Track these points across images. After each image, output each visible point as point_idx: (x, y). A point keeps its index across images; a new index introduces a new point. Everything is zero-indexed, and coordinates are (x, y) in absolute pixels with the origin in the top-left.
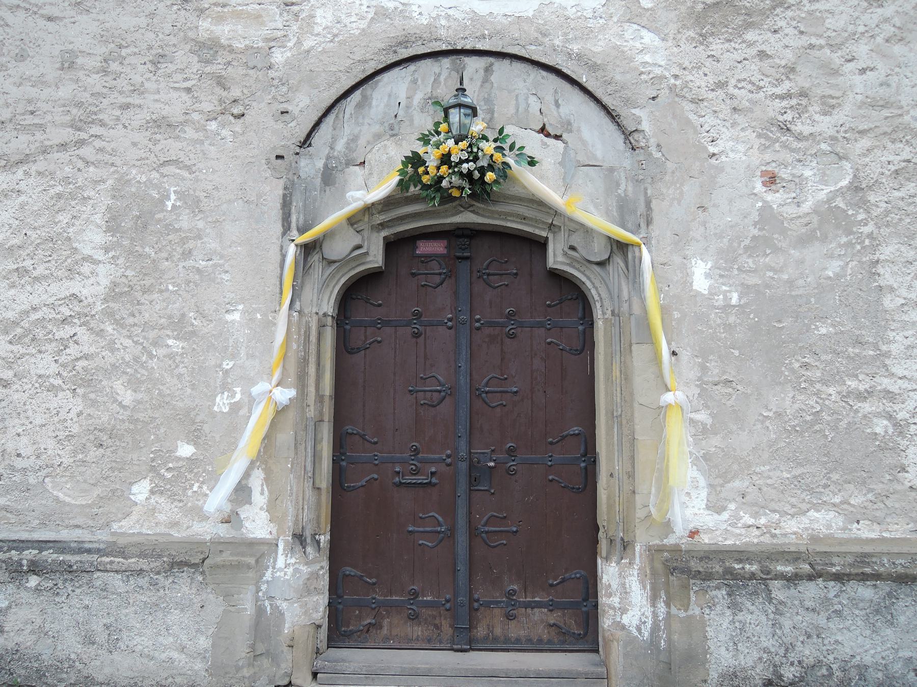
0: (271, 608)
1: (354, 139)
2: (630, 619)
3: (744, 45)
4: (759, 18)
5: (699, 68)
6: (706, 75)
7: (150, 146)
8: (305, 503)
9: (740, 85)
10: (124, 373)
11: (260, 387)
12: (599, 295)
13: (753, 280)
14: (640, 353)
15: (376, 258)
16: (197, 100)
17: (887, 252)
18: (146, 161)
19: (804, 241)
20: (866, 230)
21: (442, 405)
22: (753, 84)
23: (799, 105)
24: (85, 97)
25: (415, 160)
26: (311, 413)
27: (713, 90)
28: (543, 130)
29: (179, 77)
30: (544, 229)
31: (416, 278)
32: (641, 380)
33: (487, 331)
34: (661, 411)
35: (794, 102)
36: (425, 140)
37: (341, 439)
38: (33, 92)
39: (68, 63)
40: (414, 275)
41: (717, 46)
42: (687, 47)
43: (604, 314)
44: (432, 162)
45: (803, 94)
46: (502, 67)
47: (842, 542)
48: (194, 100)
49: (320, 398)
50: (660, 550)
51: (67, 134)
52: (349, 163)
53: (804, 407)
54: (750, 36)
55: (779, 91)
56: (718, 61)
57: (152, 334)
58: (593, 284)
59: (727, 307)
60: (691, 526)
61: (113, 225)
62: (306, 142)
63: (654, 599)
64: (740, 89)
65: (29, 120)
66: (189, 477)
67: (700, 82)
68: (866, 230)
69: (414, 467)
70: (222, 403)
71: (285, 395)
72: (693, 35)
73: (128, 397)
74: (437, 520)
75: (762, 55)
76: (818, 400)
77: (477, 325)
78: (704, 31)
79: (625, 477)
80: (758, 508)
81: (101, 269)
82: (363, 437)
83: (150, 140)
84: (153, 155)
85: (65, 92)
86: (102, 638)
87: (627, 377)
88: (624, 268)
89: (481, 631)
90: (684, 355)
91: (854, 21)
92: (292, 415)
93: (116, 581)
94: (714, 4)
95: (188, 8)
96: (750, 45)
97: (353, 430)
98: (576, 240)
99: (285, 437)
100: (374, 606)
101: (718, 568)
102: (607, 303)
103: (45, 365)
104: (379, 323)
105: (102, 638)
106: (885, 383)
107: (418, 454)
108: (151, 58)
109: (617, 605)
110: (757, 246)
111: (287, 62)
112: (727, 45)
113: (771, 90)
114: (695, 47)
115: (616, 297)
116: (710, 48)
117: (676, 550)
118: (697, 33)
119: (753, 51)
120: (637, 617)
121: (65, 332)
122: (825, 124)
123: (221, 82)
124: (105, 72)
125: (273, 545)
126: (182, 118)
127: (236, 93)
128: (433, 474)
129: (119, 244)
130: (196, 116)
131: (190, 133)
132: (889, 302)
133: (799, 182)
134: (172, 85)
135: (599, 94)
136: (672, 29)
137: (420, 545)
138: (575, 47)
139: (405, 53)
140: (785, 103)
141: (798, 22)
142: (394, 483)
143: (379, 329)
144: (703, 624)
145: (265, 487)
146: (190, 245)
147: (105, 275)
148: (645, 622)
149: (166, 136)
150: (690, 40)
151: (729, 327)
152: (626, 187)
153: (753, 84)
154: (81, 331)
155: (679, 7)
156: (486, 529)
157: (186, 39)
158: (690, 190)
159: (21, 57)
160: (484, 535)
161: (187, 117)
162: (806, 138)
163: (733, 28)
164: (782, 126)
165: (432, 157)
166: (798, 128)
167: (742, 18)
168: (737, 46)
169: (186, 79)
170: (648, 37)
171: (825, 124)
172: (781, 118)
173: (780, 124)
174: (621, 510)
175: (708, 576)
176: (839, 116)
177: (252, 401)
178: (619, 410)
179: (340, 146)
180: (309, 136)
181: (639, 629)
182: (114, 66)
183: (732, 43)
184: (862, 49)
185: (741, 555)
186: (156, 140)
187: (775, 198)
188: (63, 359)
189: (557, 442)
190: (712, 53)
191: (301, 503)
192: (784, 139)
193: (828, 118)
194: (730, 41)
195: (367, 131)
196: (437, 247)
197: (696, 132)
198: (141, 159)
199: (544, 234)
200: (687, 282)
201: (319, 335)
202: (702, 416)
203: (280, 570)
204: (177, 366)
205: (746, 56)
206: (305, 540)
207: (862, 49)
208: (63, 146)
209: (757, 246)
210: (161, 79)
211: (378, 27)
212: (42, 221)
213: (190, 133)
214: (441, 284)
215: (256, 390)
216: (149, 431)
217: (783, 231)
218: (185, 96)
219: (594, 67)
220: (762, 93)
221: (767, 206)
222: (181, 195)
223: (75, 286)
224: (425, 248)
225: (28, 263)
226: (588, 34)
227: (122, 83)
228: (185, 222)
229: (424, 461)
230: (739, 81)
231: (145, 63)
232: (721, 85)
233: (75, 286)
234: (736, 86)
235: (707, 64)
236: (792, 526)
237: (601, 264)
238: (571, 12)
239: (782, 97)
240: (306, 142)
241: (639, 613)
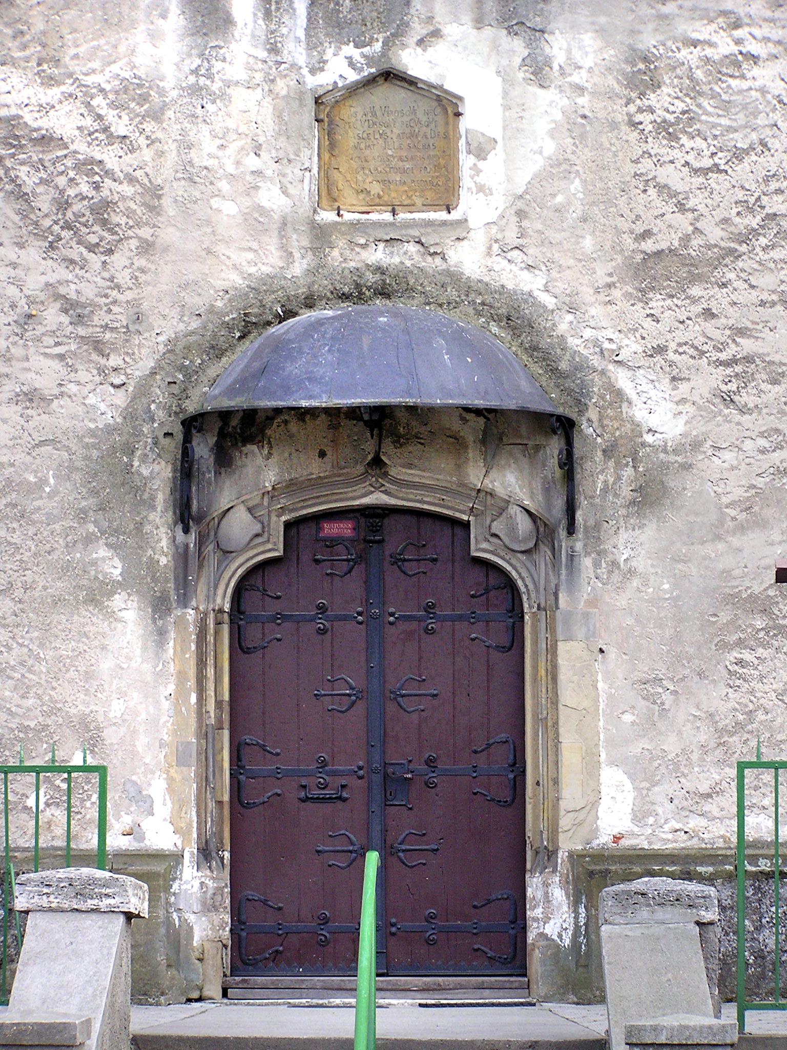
0: (180, 920)
2: (551, 929)
3: (688, 301)
4: (705, 270)
5: (636, 330)
6: (643, 338)
7: (23, 423)
8: (208, 815)
9: (681, 350)
10: (9, 677)
12: (526, 586)
18: (19, 441)
21: (351, 712)
22: (696, 348)
23: (744, 372)
27: (651, 356)
29: (50, 341)
30: (463, 512)
31: (321, 565)
33: (403, 626)
35: (739, 369)
37: (238, 751)
40: (317, 561)
41: (657, 302)
43: (531, 607)
48: (69, 369)
49: (219, 704)
53: (737, 706)
55: (723, 356)
56: (658, 321)
58: (519, 574)
60: (615, 832)
63: (576, 904)
64: (680, 354)
66: (86, 788)
72: (631, 290)
74: (349, 838)
75: (708, 314)
76: (752, 698)
77: (392, 619)
78: (643, 285)
79: (551, 783)
82: (263, 747)
83: (21, 416)
84: (26, 434)
88: (552, 557)
94: (655, 253)
95: (55, 257)
96: (695, 301)
97: (251, 740)
100: (280, 932)
102: (533, 595)
104: (279, 619)
107: (326, 765)
108: (16, 318)
109: (540, 916)
112: (669, 302)
113: (715, 355)
114: (633, 305)
115: (542, 589)
116: (650, 306)
118: (636, 289)
119: (698, 309)
120: (558, 925)
125: (176, 858)
126: (56, 391)
128: (343, 787)
130: (72, 388)
134: (42, 350)
137: (330, 866)
140: (729, 371)
141: (750, 274)
142: (300, 799)
143: (279, 624)
145: (167, 797)
148: (566, 929)
149: (40, 411)
150: (628, 295)
153: (696, 348)
155: (615, 256)
156: (404, 847)
160: (401, 854)
161: (63, 389)
162: (750, 411)
163: (676, 282)
164: (725, 397)
167: (687, 269)
168: (679, 303)
169: (58, 344)
172: (724, 388)
173: (723, 394)
174: (545, 818)
178: (545, 712)
181: (560, 936)
183: (675, 300)
186: (28, 416)
189: (483, 750)
190: (652, 312)
191: (203, 816)
192: (727, 411)
193: (777, 388)
194: (672, 296)
196: (343, 529)
198: (14, 438)
199: (465, 518)
201: (217, 633)
203: (187, 882)
204: (68, 670)
205: (690, 314)
206: (210, 853)
210: (30, 343)
214: (350, 571)
216: (41, 740)
218: (56, 365)
220: (705, 359)
224: (331, 529)
229: (334, 774)
230: (680, 345)
231: (9, 324)
232: (660, 350)
234: (676, 351)
235: (645, 325)
239: (727, 364)
241: (561, 920)
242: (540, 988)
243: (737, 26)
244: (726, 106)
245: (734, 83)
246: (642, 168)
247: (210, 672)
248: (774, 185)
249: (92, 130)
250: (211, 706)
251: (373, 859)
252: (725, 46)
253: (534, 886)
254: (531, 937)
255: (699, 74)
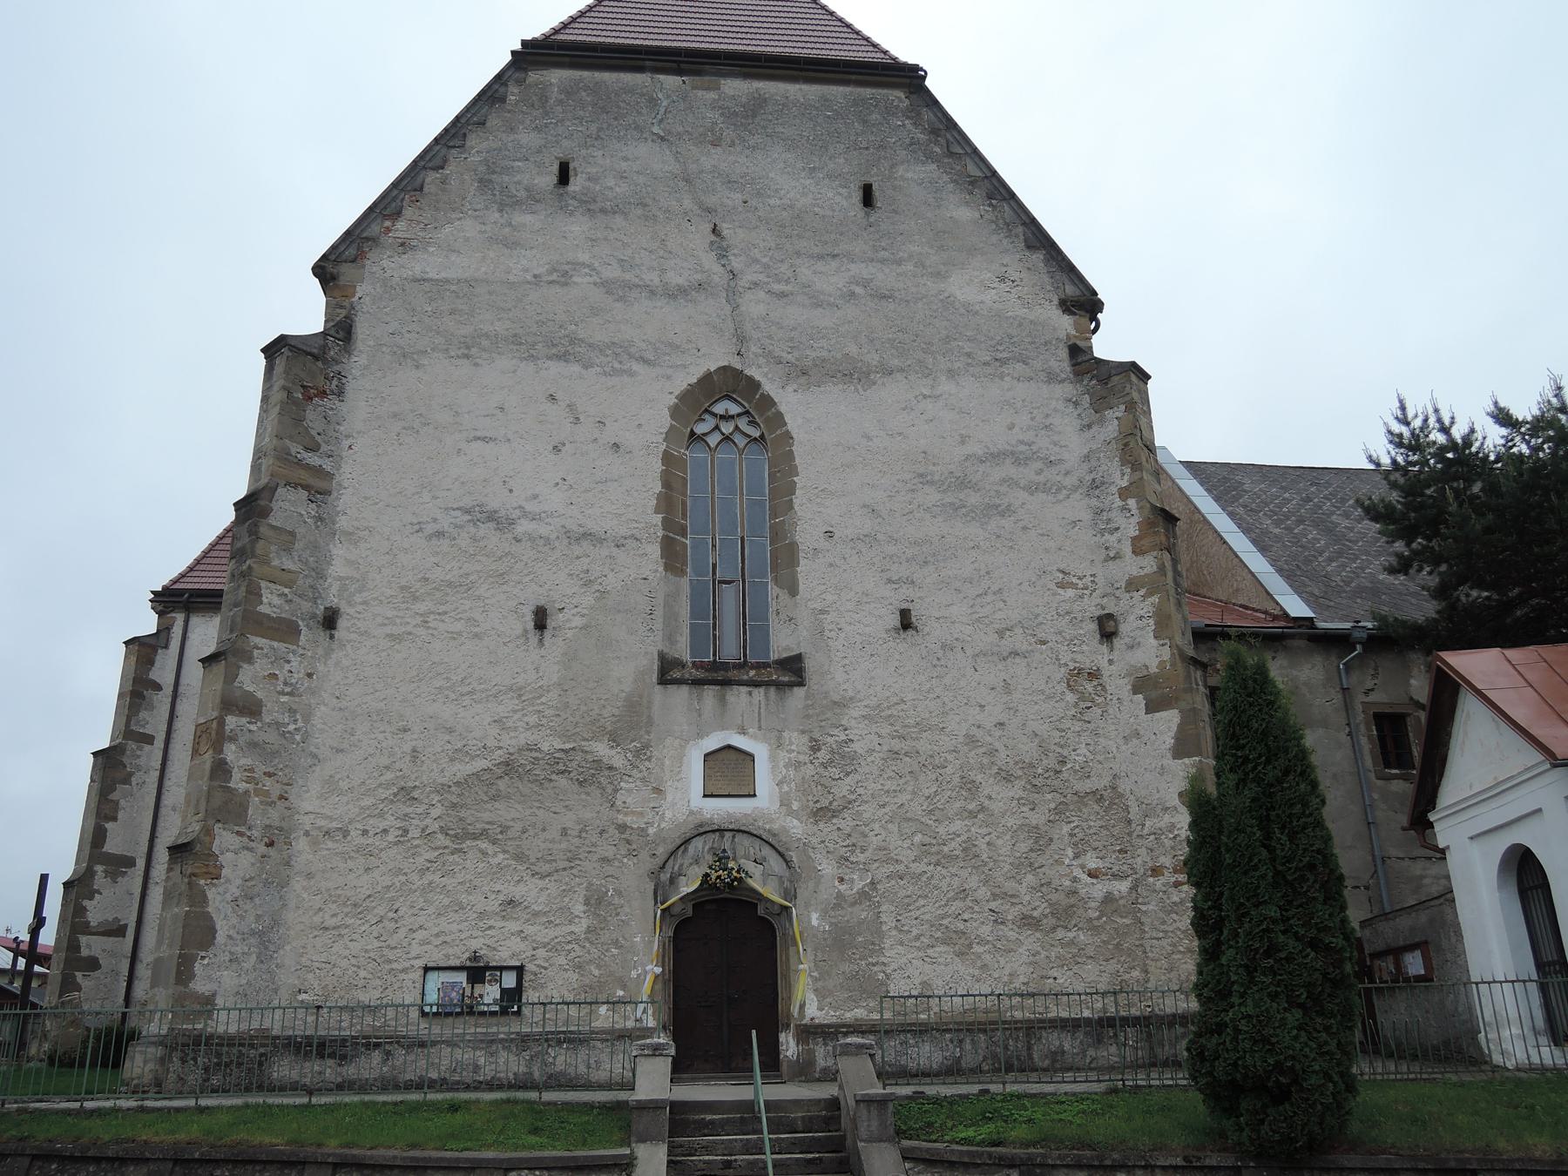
1: (682, 865)
2: (789, 1053)
11: (649, 967)
13: (833, 920)
14: (792, 949)
15: (690, 913)
16: (618, 849)
17: (883, 908)
19: (853, 904)
20: (876, 899)
24: (573, 848)
25: (707, 875)
26: (667, 977)
28: (755, 861)
32: (792, 960)
34: (797, 971)
36: (710, 867)
38: (551, 846)
39: (564, 832)
41: (821, 825)
42: (810, 826)
44: (713, 877)
45: (854, 845)
46: (739, 837)
47: (866, 1020)
50: (800, 1025)
51: (567, 864)
52: (680, 875)
54: (834, 821)
57: (605, 947)
59: (824, 931)
61: (587, 902)
62: (663, 867)
65: (550, 858)
67: (814, 841)
68: (876, 899)
69: (1000, 348)
70: (634, 974)
71: (658, 970)
73: (596, 972)
75: (839, 829)
80: (836, 1009)
81: (583, 921)
85: (564, 845)
86: (594, 1066)
87: (787, 959)
89: (734, 1065)
90: (809, 950)
91: (874, 814)
92: (660, 978)
93: (598, 1044)
98: (768, 905)
99: (659, 986)
101: (820, 1030)
103: (562, 960)
105: (594, 1066)
106: (883, 959)
110: (837, 906)
111: (655, 833)
117: (806, 1025)
121: (570, 947)
122: (862, 857)
123: (628, 842)
124: (580, 837)
127: (634, 846)
129: (589, 910)
131: (617, 864)
132: (884, 928)
133: (852, 881)
135: (777, 846)
136: (804, 818)
138: (767, 827)
139: (702, 830)
144: (814, 1051)
146: (619, 910)
147: (585, 923)
151: (825, 939)
152: (787, 884)
154: (576, 946)
157: (613, 823)
158: (811, 884)
159: (544, 830)
165: (714, 875)
166: (851, 859)
170: (795, 821)
171: (862, 857)
175: (816, 1033)
176: (867, 854)
177: (646, 973)
179: (676, 868)
180: (664, 864)
182: (584, 835)
184: (876, 826)
185: (829, 1026)
187: (842, 888)
188: (569, 958)
195: (686, 863)
197: (813, 861)
200: (810, 922)
202: (815, 974)
207: (876, 826)
208: (565, 869)
209: (837, 906)
211: (690, 818)
212: (558, 900)
213: (617, 864)
215: (647, 968)
217: (846, 901)
218: (614, 848)
219: (774, 835)
221: (839, 891)
222: (614, 890)
223: (572, 928)
225: (552, 918)
226: (772, 821)
227: (587, 842)
228: (616, 901)
232: (823, 842)
233: (572, 928)
236: (848, 1015)
237: (778, 914)
238: (765, 811)
240: (663, 867)
242: (785, 1078)
243: (846, 730)
244: (843, 757)
245: (846, 749)
246: (815, 778)
247: (667, 959)
248: (860, 784)
249: (499, 553)
250: (667, 972)
251: (754, 1032)
252: (843, 737)
253: (782, 1037)
254: (782, 1056)
255: (834, 746)
